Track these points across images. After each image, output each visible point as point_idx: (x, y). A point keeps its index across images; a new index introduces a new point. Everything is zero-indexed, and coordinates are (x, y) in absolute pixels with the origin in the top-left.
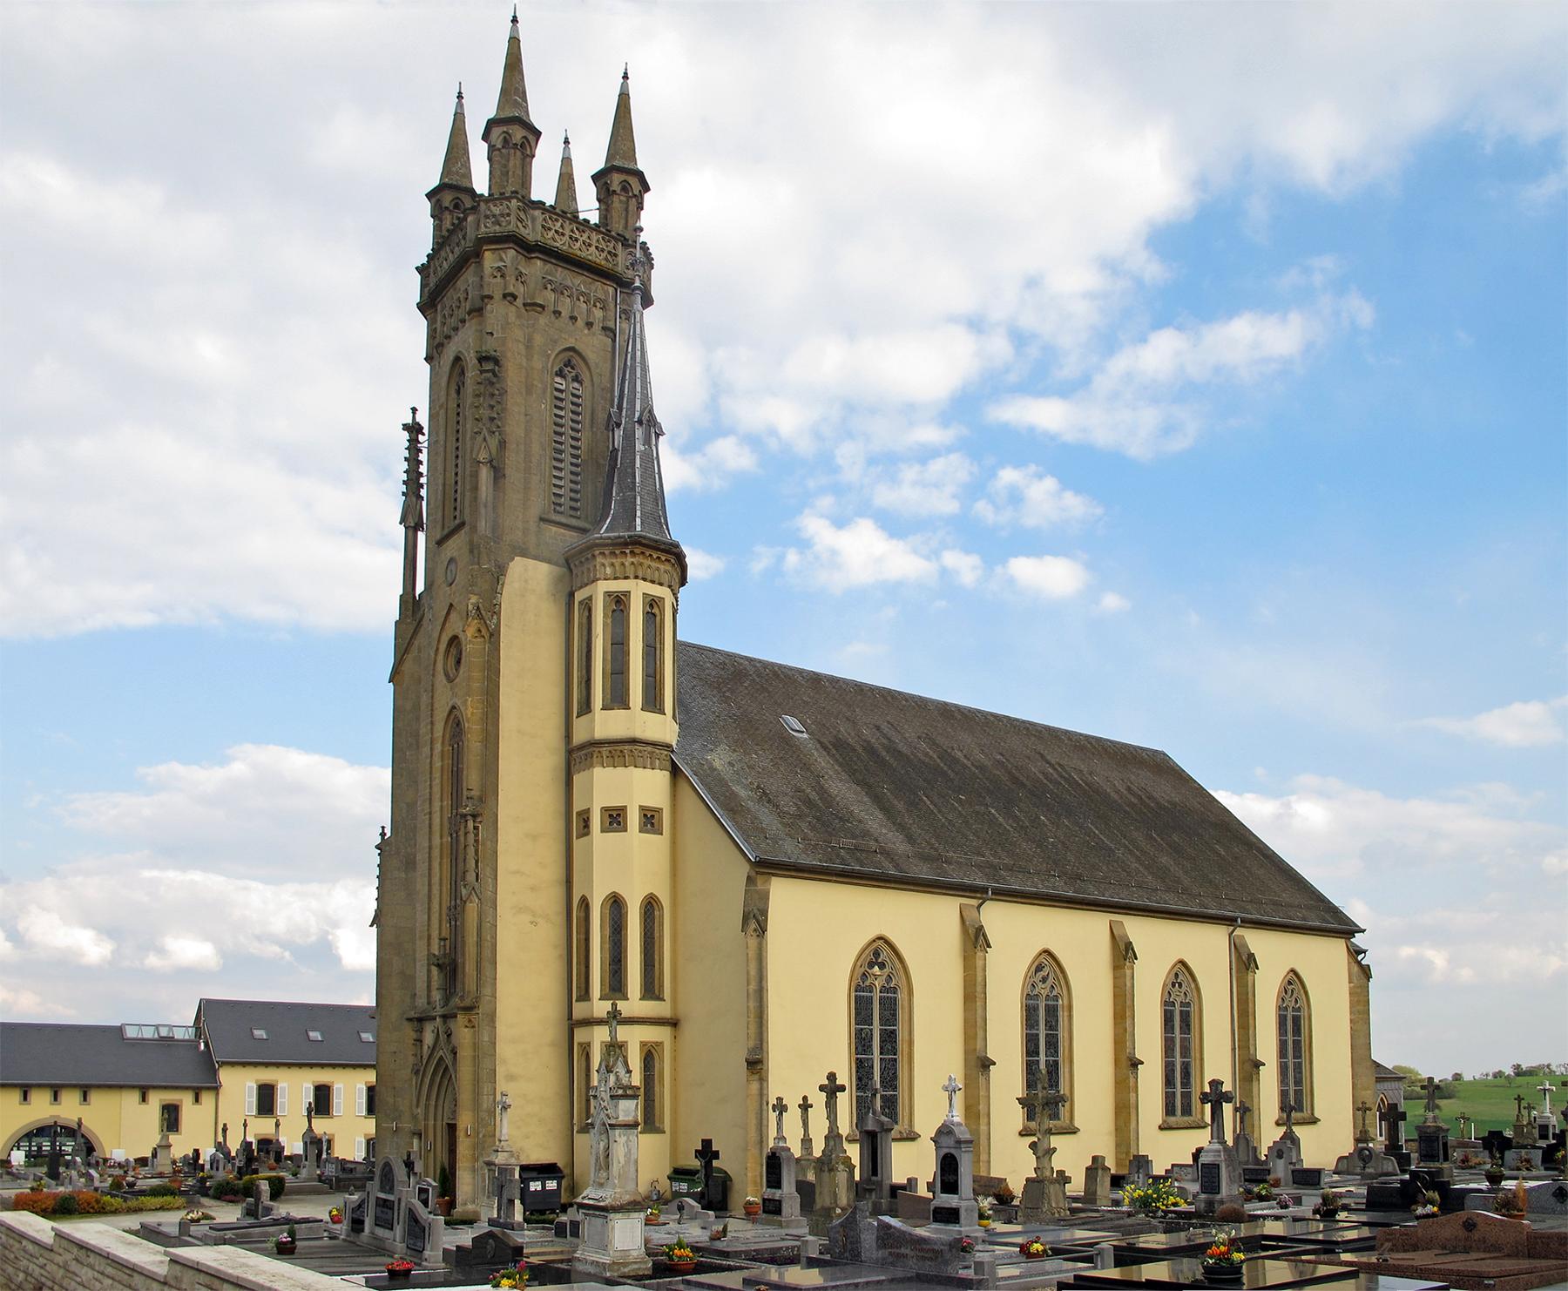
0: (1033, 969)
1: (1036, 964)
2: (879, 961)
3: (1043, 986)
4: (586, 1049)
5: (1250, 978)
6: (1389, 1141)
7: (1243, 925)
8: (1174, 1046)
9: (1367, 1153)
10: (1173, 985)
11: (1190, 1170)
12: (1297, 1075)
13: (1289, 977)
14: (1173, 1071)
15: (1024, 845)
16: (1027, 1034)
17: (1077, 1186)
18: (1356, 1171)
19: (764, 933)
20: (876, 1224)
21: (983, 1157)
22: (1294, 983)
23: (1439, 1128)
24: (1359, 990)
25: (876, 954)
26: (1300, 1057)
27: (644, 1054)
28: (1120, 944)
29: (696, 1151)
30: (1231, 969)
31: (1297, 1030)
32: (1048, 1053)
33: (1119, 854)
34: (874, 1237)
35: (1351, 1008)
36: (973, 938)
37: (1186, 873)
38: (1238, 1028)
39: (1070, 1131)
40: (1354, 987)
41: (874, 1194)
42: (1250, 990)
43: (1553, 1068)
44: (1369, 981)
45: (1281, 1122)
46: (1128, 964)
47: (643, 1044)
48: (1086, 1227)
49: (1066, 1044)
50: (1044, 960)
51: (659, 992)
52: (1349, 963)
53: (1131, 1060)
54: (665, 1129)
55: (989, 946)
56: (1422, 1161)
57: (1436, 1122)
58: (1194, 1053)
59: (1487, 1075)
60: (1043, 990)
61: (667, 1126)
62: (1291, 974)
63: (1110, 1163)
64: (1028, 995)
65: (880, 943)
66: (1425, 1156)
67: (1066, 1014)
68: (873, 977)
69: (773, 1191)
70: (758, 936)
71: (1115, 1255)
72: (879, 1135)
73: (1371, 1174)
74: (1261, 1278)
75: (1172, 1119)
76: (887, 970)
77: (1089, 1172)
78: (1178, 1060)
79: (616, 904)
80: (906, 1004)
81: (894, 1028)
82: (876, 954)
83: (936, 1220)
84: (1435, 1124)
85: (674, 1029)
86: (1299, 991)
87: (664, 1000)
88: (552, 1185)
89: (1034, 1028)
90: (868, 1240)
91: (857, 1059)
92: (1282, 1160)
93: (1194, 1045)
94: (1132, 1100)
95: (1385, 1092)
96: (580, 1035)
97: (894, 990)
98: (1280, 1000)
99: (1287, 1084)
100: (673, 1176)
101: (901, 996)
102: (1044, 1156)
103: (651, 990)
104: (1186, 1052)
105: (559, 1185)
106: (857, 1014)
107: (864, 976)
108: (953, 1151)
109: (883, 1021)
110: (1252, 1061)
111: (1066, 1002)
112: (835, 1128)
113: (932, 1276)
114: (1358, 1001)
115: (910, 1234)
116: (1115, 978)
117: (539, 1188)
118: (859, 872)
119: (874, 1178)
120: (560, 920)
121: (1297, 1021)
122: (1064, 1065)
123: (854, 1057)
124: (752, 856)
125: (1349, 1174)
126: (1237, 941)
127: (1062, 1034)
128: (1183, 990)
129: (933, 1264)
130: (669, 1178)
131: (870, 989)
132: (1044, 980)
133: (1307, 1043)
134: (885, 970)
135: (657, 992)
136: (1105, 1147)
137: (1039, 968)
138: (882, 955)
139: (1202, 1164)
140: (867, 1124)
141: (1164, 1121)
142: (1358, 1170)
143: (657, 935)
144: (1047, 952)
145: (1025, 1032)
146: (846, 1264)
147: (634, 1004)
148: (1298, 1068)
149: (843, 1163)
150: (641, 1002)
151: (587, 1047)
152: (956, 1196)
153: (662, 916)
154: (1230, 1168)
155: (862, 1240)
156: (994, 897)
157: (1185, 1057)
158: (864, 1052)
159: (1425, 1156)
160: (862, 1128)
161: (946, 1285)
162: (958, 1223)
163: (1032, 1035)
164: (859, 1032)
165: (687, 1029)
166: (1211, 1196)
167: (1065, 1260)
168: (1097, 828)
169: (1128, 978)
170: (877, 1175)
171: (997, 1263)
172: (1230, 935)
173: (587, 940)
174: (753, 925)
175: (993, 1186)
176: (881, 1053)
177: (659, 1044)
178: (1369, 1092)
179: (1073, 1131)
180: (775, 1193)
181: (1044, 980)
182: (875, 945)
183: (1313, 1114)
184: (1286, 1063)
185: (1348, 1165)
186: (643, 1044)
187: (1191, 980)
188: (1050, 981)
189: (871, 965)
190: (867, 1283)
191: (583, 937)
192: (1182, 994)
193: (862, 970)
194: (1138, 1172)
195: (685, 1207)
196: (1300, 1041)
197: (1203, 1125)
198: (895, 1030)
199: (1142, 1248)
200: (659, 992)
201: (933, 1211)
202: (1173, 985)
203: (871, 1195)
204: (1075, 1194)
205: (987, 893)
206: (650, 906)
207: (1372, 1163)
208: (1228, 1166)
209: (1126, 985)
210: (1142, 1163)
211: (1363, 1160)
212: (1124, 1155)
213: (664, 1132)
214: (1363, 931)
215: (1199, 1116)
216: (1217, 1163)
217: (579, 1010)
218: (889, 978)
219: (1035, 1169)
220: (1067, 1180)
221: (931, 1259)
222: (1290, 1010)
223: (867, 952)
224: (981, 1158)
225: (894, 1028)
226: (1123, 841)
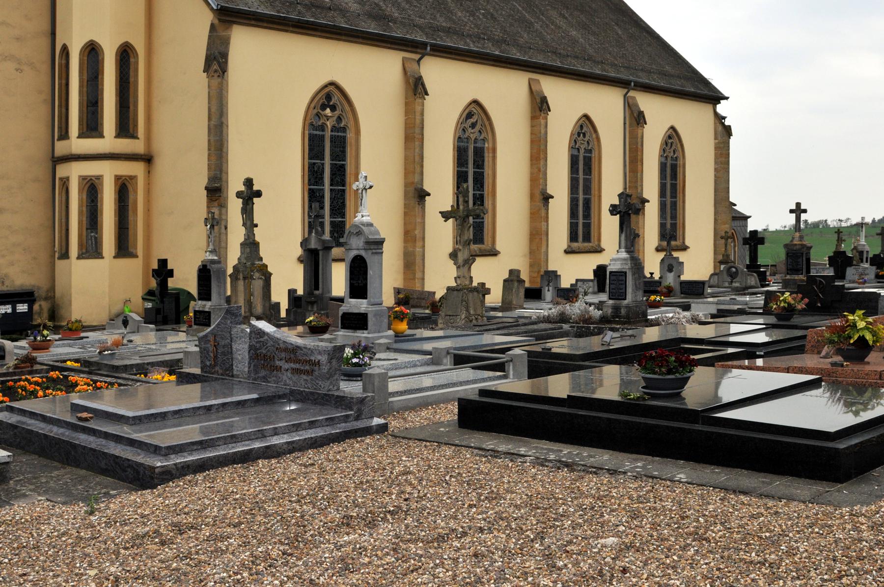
0: (464, 115)
1: (467, 111)
2: (331, 103)
3: (472, 131)
4: (65, 182)
5: (640, 131)
6: (832, 228)
7: (635, 88)
8: (578, 185)
9: (734, 270)
10: (579, 136)
11: (591, 284)
12: (673, 212)
13: (669, 133)
14: (577, 205)
15: (460, 14)
16: (457, 171)
17: (494, 298)
18: (724, 285)
19: (224, 73)
20: (248, 330)
21: (418, 275)
22: (672, 139)
23: (803, 246)
24: (722, 145)
25: (329, 97)
26: (676, 197)
27: (118, 187)
28: (537, 97)
29: (154, 270)
30: (625, 124)
31: (674, 176)
32: (476, 188)
33: (537, 26)
34: (246, 346)
35: (715, 159)
36: (413, 87)
37: (590, 45)
38: (629, 172)
39: (491, 253)
40: (719, 143)
41: (315, 306)
42: (639, 140)
43: (829, 222)
44: (730, 138)
45: (659, 248)
46: (543, 115)
47: (118, 178)
48: (505, 331)
49: (491, 181)
50: (473, 109)
51: (134, 131)
52: (715, 123)
53: (543, 195)
54: (138, 254)
55: (427, 94)
56: (788, 274)
57: (801, 241)
58: (594, 191)
59: (785, 227)
60: (472, 134)
61: (140, 251)
62: (671, 130)
63: (524, 276)
64: (459, 138)
65: (331, 88)
66: (791, 270)
67: (491, 155)
68: (324, 118)
69: (204, 303)
70: (219, 76)
71: (529, 361)
72: (321, 253)
73: (737, 287)
74: (623, 371)
75: (575, 245)
76: (337, 113)
77: (506, 283)
78: (581, 197)
79: (92, 51)
80: (353, 142)
81: (343, 163)
82: (329, 97)
83: (345, 326)
84: (801, 243)
85: (147, 164)
86: (677, 144)
87: (138, 139)
88: (22, 308)
89: (464, 166)
90: (241, 351)
91: (310, 189)
92: (672, 274)
93: (594, 186)
94: (544, 228)
95: (735, 228)
96: (62, 171)
97: (344, 129)
98: (662, 151)
99: (665, 219)
100: (145, 297)
101: (350, 135)
102: (464, 265)
103: (125, 128)
104: (587, 189)
105: (30, 308)
106: (310, 150)
107: (318, 115)
108: (363, 253)
109: (334, 157)
110: (639, 198)
111: (491, 145)
112: (251, 235)
113: (307, 393)
114: (721, 154)
115: (284, 342)
116: (532, 126)
117: (9, 311)
118: (313, 23)
119: (316, 292)
120: (45, 68)
121: (674, 168)
122: (488, 198)
123: (307, 187)
124: (215, 4)
125: (718, 288)
126: (630, 101)
127: (487, 171)
128: (586, 139)
129: (309, 378)
130: (143, 299)
131: (322, 128)
132: (473, 126)
133: (681, 185)
134: (336, 112)
135: (131, 130)
136: (520, 263)
137: (470, 115)
138: (343, 120)
139: (611, 272)
140: (310, 244)
141: (569, 246)
142: (727, 284)
143: (132, 80)
144: (476, 102)
145: (456, 169)
146: (216, 379)
147: (109, 141)
148: (674, 205)
149: (258, 271)
150: (116, 139)
151: (67, 183)
152: (364, 301)
153: (137, 63)
154: (637, 275)
155: (234, 350)
156: (432, 53)
157: (586, 194)
158: (316, 183)
159: (791, 270)
160: (306, 246)
161: (323, 405)
162: (366, 329)
163: (462, 172)
164: (311, 167)
165: (162, 165)
166: (618, 302)
167: (473, 368)
168: (520, 5)
169: (543, 127)
170: (318, 290)
171: (391, 374)
172: (625, 96)
173: (67, 84)
174: (215, 66)
175: (424, 299)
176: (331, 185)
177: (133, 178)
178: (727, 226)
179: (494, 253)
180: (205, 305)
181: (473, 126)
182: (327, 90)
183: (684, 243)
184: (665, 202)
185: (718, 280)
186: (118, 178)
187: (593, 132)
188: (478, 127)
189: (324, 107)
190: (224, 405)
191: (64, 82)
192: (586, 143)
193: (315, 111)
194: (548, 285)
195: (130, 322)
196: (676, 184)
197: (599, 250)
198: (344, 165)
199: (804, 326)
200: (134, 131)
201: (341, 317)
202: (579, 136)
203: (312, 307)
204: (494, 305)
205: (426, 49)
206: (125, 54)
207: (737, 279)
208: (633, 274)
209: (540, 133)
210: (552, 277)
211: (731, 276)
212: (536, 274)
213: (137, 257)
214: (727, 98)
215: (596, 243)
216: (624, 270)
217: (61, 148)
218: (339, 119)
219: (455, 278)
220: (488, 291)
221: (307, 373)
222: (669, 159)
223: (320, 96)
224: (417, 276)
225: (343, 163)
226: (541, 17)
